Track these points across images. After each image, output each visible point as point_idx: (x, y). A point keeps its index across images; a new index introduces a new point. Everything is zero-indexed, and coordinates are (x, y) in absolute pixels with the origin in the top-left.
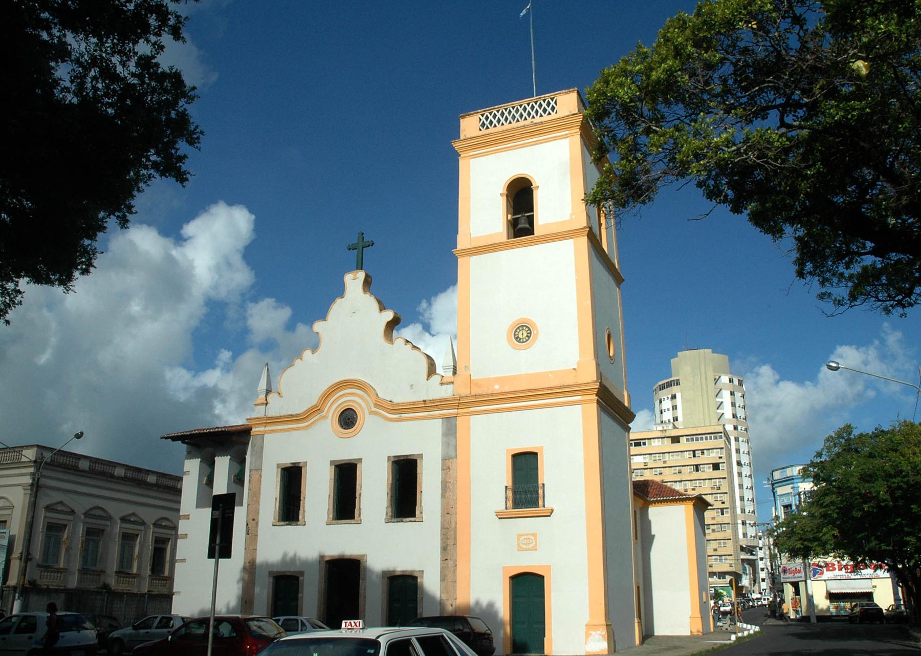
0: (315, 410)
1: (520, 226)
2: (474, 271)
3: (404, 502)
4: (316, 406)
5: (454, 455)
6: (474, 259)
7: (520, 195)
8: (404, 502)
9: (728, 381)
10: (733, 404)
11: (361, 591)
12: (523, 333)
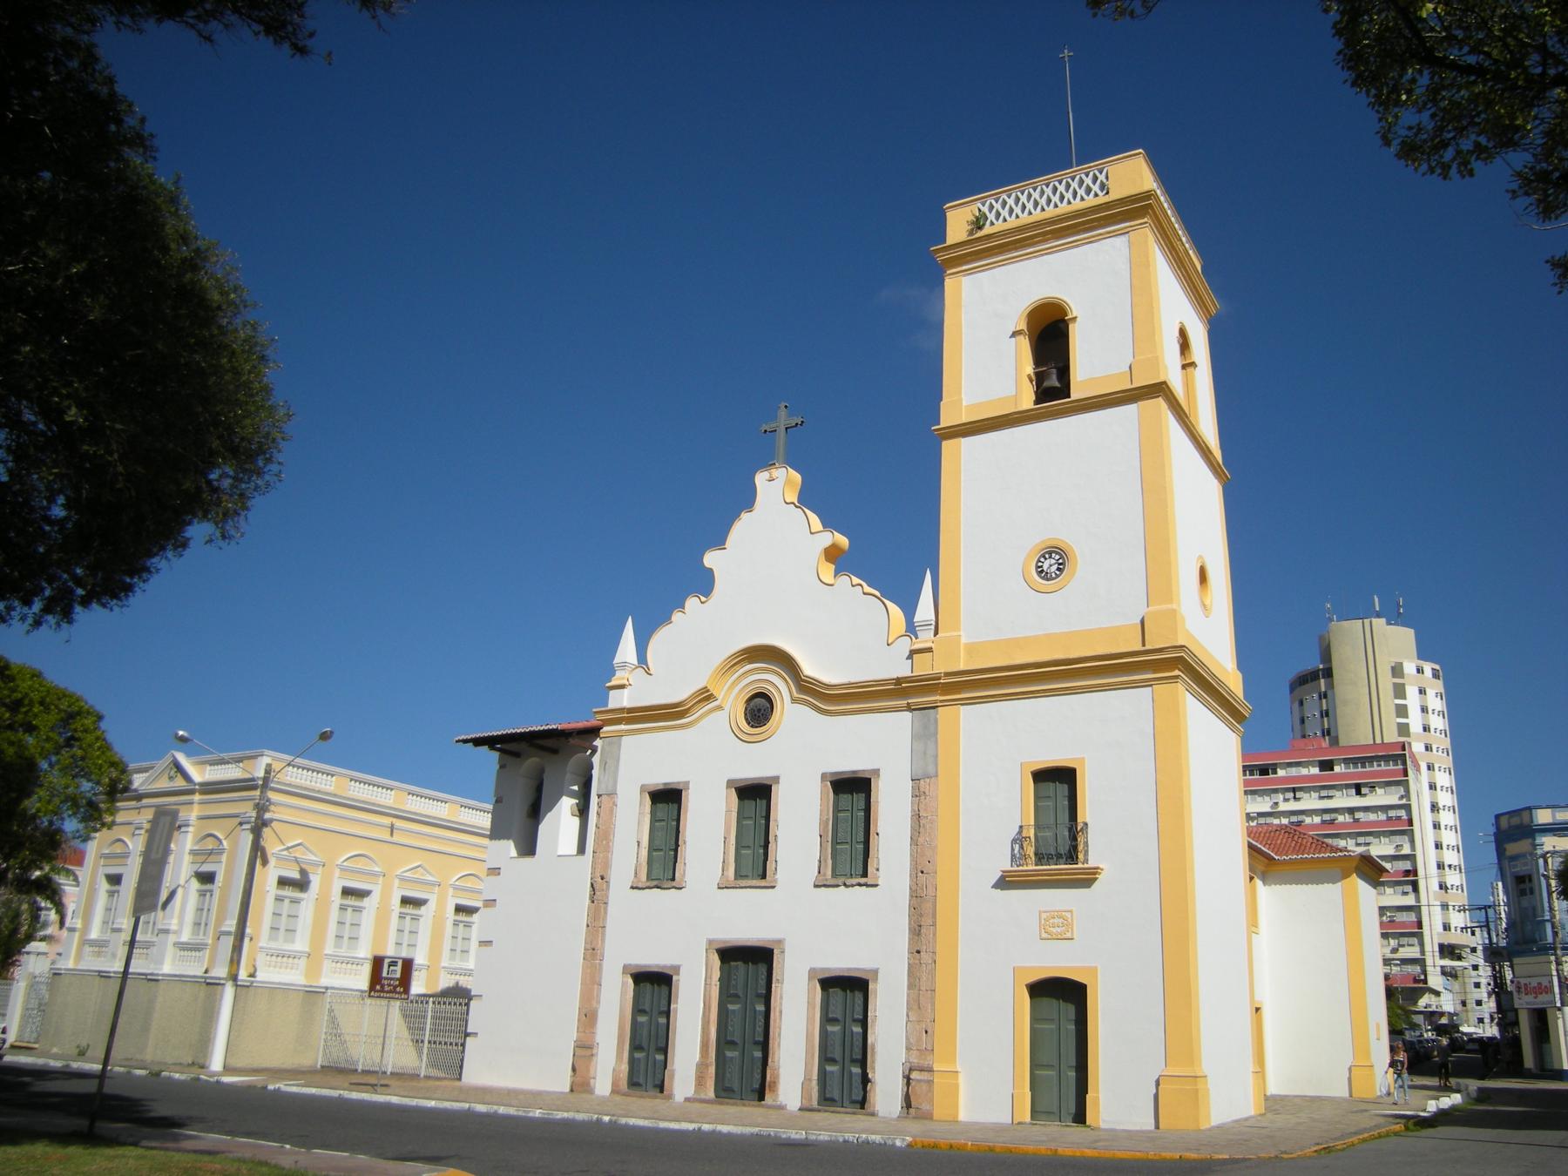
0: (705, 696)
1: (1047, 384)
2: (970, 471)
3: (851, 853)
4: (705, 689)
5: (931, 770)
6: (966, 443)
7: (1049, 335)
8: (851, 853)
9: (1414, 671)
10: (1424, 710)
11: (1137, 1160)
12: (1053, 562)
